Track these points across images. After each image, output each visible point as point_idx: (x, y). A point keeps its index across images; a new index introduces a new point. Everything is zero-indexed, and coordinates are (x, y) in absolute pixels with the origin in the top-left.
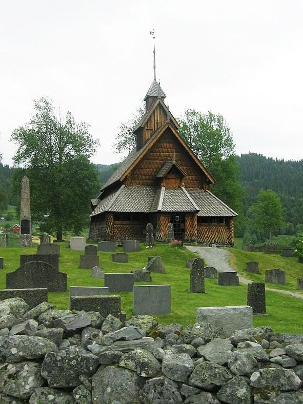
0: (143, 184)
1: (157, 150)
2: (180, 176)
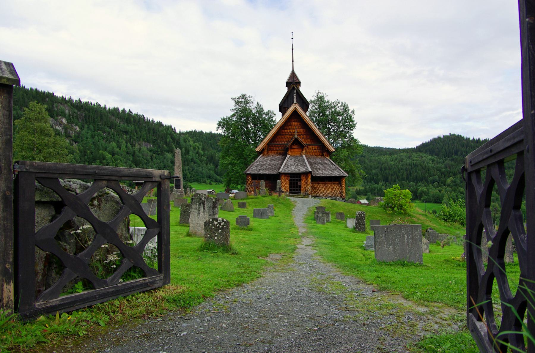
0: (277, 153)
1: (287, 128)
2: (302, 147)
